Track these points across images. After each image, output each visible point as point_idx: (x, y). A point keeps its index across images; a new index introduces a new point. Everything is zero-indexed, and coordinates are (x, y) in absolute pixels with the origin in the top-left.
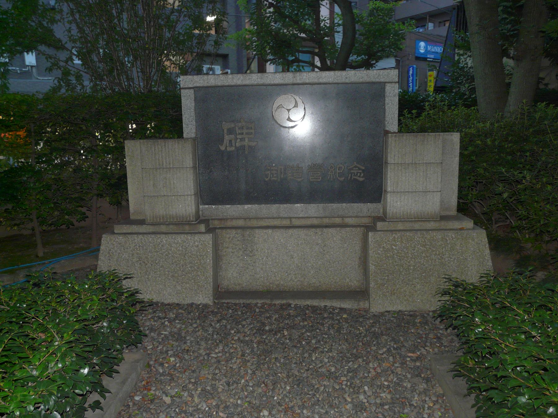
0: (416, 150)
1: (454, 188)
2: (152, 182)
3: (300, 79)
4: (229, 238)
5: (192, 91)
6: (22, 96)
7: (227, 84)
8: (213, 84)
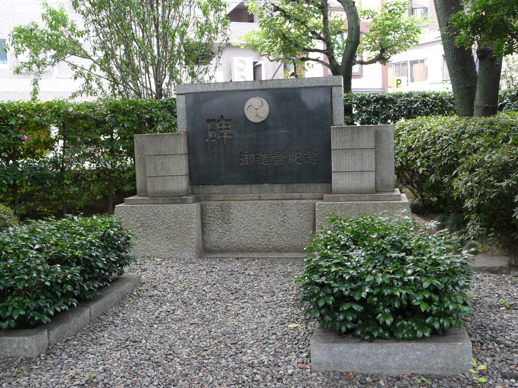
0: (353, 138)
1: (391, 169)
2: (153, 166)
3: (266, 86)
4: (211, 209)
5: (184, 96)
6: (435, 95)
7: (210, 90)
8: (200, 91)
